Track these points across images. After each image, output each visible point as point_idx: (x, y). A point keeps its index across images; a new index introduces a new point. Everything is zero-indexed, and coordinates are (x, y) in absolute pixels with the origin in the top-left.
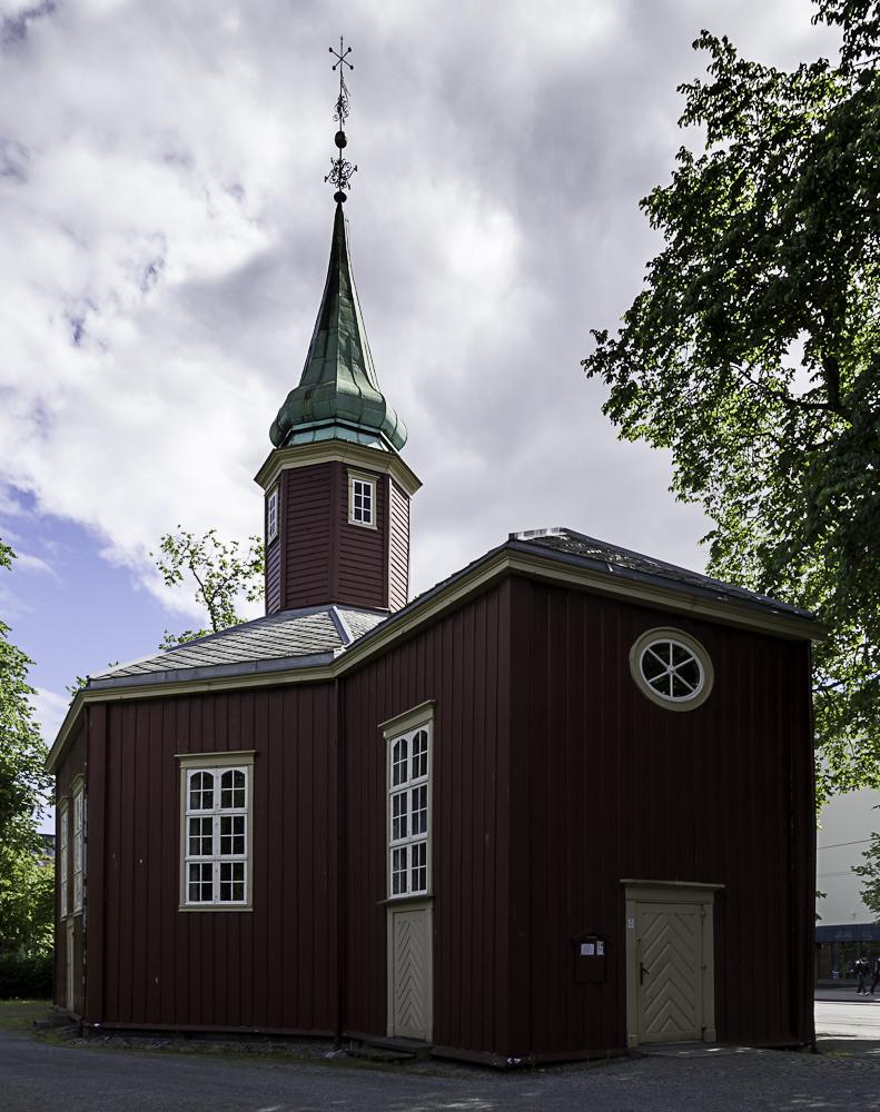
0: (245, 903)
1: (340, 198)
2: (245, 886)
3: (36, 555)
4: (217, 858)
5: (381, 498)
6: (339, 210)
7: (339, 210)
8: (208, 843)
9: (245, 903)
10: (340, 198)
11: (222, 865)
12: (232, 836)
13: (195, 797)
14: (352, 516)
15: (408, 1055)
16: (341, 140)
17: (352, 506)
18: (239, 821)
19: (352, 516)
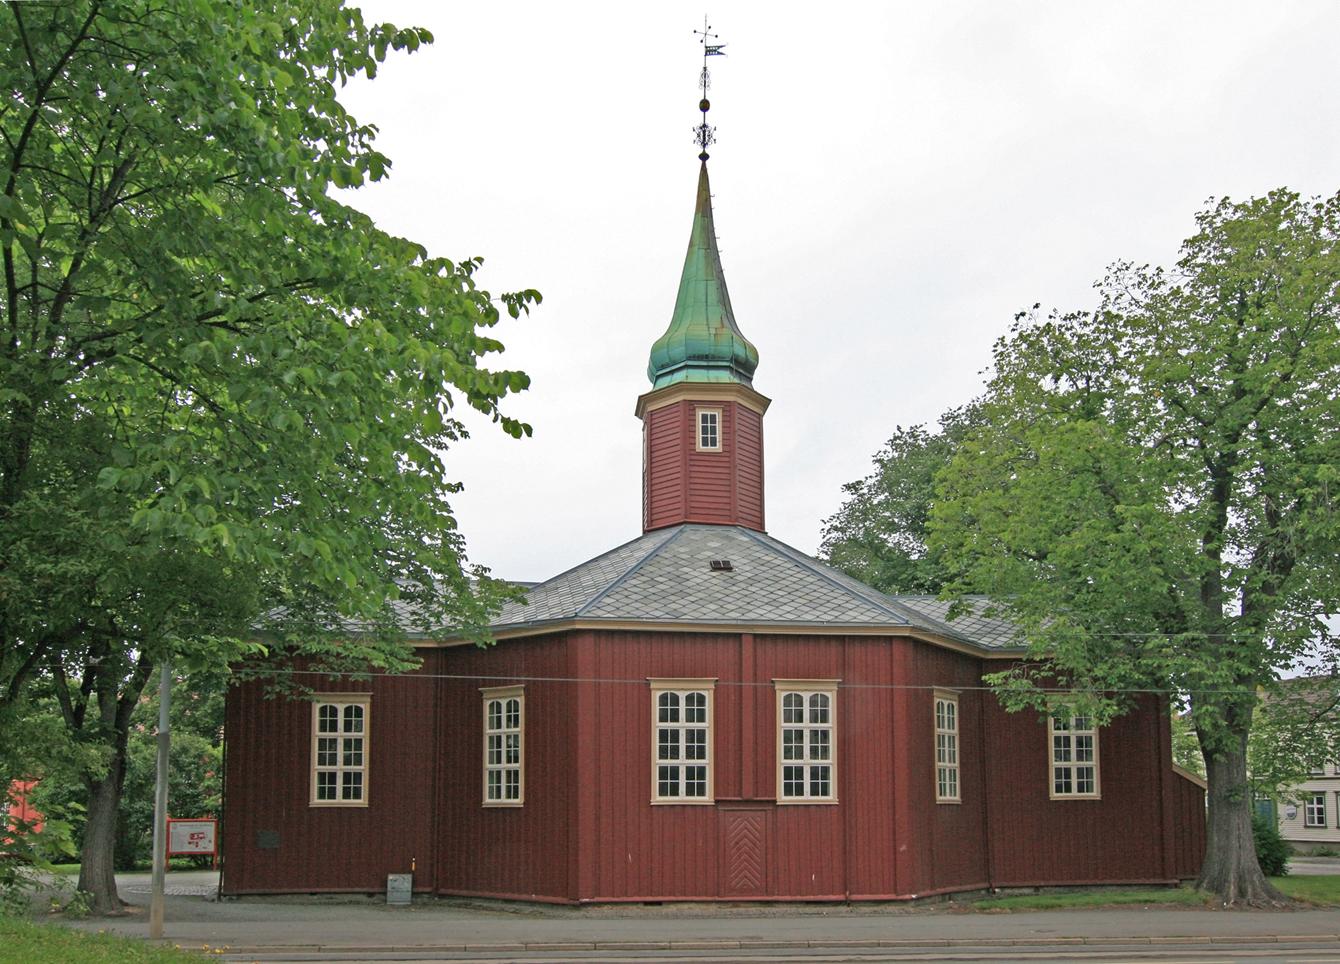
0: (362, 802)
1: (704, 157)
2: (707, 748)
3: (1164, 728)
4: (1074, 764)
5: (728, 442)
6: (704, 170)
7: (704, 170)
8: (1068, 753)
9: (362, 802)
10: (704, 157)
11: (811, 768)
12: (820, 781)
13: (825, 776)
14: (719, 419)
15: (212, 320)
16: (705, 106)
17: (719, 426)
18: (788, 755)
19: (719, 419)
